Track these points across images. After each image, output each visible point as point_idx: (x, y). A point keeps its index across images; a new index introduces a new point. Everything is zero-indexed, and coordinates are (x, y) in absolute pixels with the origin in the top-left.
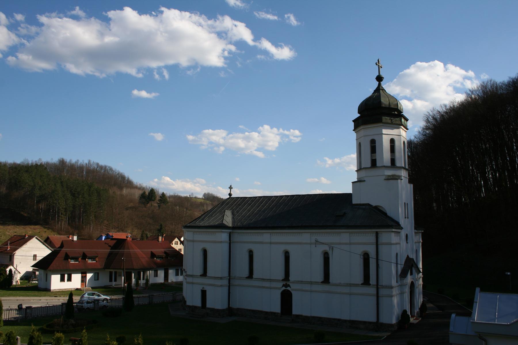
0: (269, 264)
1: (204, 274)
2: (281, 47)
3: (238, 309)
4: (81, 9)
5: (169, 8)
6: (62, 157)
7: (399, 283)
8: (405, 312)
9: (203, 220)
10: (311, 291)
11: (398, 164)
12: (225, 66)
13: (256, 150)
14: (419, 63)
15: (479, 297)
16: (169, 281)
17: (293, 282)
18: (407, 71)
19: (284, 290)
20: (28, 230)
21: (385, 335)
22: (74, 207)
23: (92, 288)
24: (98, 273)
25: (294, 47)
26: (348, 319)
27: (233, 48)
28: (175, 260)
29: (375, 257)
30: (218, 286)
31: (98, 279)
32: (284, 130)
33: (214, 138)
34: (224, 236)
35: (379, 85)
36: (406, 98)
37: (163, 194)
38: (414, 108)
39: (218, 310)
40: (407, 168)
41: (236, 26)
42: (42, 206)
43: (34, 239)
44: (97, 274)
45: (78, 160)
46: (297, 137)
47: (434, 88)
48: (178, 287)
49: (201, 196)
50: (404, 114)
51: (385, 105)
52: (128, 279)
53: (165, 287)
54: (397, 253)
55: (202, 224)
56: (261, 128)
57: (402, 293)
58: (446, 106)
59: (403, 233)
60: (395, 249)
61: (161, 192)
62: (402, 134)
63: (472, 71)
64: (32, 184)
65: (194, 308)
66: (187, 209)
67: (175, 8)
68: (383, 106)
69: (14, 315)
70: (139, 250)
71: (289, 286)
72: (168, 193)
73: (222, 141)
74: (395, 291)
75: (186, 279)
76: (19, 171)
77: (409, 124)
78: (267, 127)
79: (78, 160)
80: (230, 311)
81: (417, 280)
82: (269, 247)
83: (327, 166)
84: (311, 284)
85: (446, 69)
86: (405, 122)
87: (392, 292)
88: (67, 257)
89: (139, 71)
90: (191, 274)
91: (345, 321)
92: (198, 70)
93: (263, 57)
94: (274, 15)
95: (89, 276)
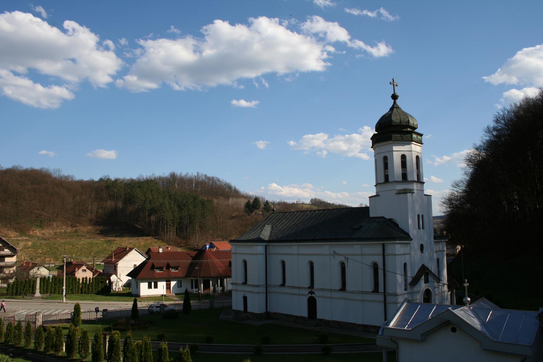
0: (298, 275)
1: (245, 283)
3: (275, 313)
4: (175, 28)
6: (173, 171)
10: (331, 298)
11: (409, 178)
13: (359, 152)
17: (317, 290)
19: (310, 297)
20: (133, 241)
22: (181, 218)
23: (176, 294)
24: (181, 281)
26: (361, 323)
27: (331, 49)
31: (181, 287)
34: (260, 249)
35: (395, 103)
39: (256, 314)
42: (153, 218)
43: (134, 250)
44: (179, 282)
45: (187, 173)
49: (308, 202)
52: (207, 286)
56: (360, 129)
59: (415, 244)
64: (144, 199)
65: (238, 312)
68: (394, 124)
69: (93, 316)
70: (217, 260)
71: (314, 293)
76: (133, 187)
79: (187, 173)
80: (268, 315)
86: (419, 137)
88: (153, 267)
91: (359, 325)
95: (173, 283)
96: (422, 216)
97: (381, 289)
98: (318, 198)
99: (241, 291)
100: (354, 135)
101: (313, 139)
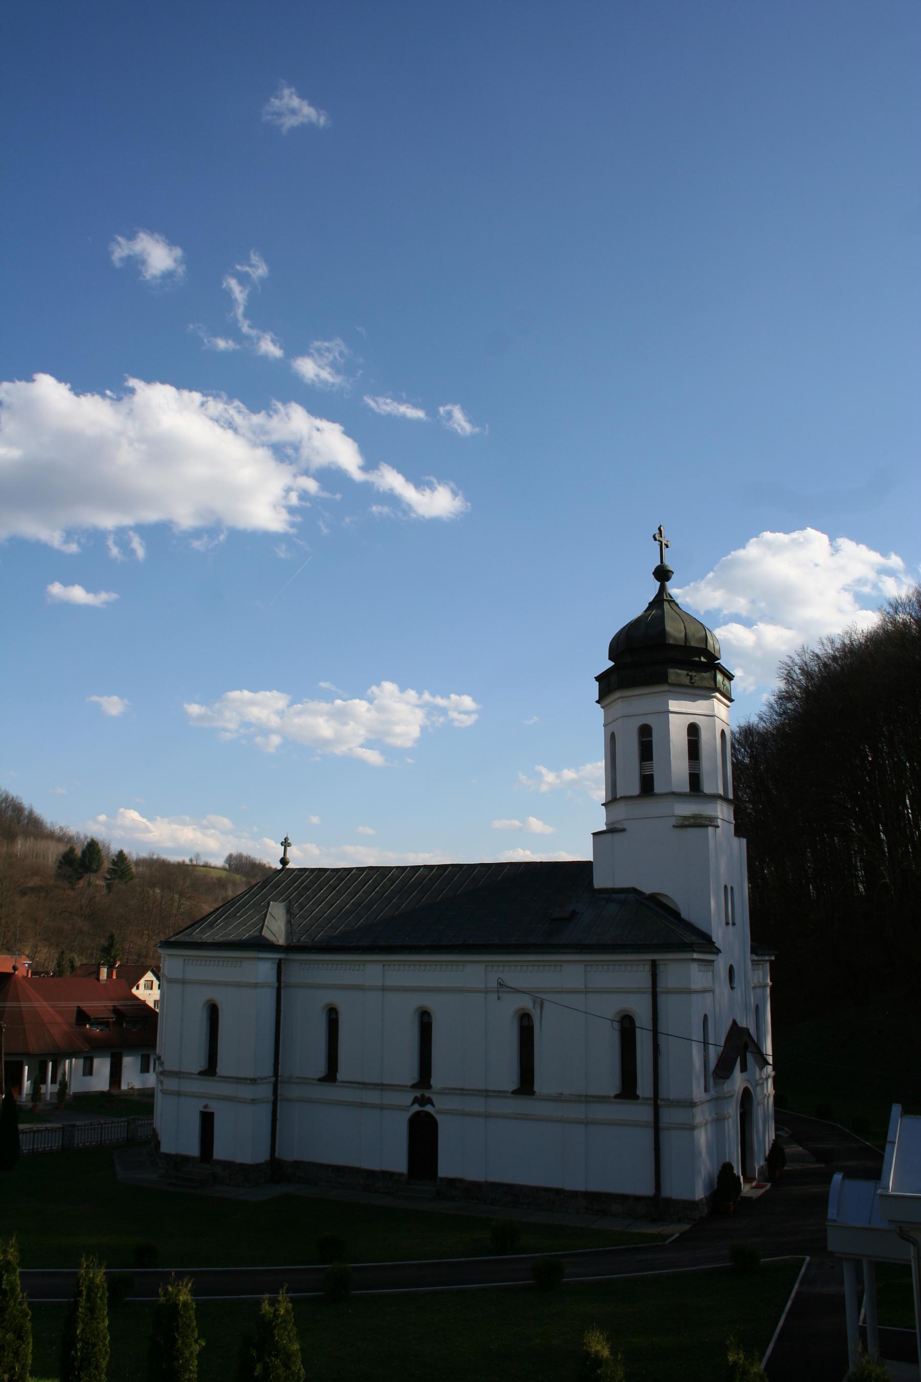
0: (379, 1042)
1: (210, 1070)
2: (433, 489)
3: (297, 1164)
5: (149, 379)
7: (712, 1092)
8: (727, 1168)
9: (211, 925)
10: (487, 1116)
11: (707, 788)
12: (293, 531)
13: (362, 746)
14: (768, 535)
15: (901, 1128)
16: (124, 1087)
18: (741, 553)
19: (417, 1114)
21: (675, 1230)
25: (461, 487)
26: (581, 1187)
27: (311, 485)
28: (136, 1030)
29: (650, 1027)
30: (244, 1102)
32: (433, 695)
33: (256, 713)
34: (262, 969)
35: (662, 589)
36: (737, 619)
37: (121, 853)
38: (759, 644)
39: (243, 1167)
40: (731, 796)
41: (318, 430)
46: (467, 713)
47: (793, 599)
48: (143, 1103)
50: (723, 662)
51: (675, 639)
53: (111, 1102)
54: (706, 1016)
55: (207, 937)
56: (374, 688)
57: (719, 1120)
58: (832, 642)
59: (721, 963)
60: (699, 1006)
61: (115, 848)
62: (716, 713)
63: (897, 554)
66: (182, 894)
67: (163, 382)
68: (671, 642)
71: (430, 1101)
72: (134, 853)
73: (275, 721)
74: (702, 1115)
75: (161, 1082)
77: (736, 687)
78: (389, 687)
80: (277, 1169)
81: (761, 1084)
82: (379, 998)
83: (544, 788)
84: (487, 1096)
85: (836, 550)
86: (726, 682)
87: (693, 1116)
89: (70, 535)
90: (176, 1069)
91: (574, 1194)
92: (222, 537)
93: (386, 510)
94: (416, 406)
96: (732, 888)
97: (644, 1087)
98: (245, 854)
99: (194, 1095)
100: (357, 701)
101: (252, 703)
